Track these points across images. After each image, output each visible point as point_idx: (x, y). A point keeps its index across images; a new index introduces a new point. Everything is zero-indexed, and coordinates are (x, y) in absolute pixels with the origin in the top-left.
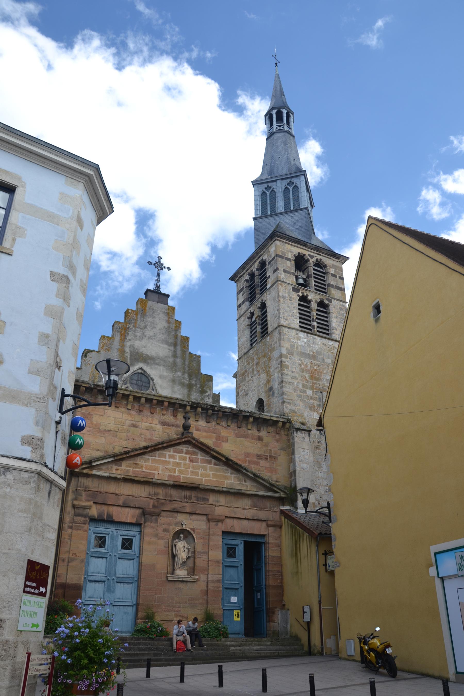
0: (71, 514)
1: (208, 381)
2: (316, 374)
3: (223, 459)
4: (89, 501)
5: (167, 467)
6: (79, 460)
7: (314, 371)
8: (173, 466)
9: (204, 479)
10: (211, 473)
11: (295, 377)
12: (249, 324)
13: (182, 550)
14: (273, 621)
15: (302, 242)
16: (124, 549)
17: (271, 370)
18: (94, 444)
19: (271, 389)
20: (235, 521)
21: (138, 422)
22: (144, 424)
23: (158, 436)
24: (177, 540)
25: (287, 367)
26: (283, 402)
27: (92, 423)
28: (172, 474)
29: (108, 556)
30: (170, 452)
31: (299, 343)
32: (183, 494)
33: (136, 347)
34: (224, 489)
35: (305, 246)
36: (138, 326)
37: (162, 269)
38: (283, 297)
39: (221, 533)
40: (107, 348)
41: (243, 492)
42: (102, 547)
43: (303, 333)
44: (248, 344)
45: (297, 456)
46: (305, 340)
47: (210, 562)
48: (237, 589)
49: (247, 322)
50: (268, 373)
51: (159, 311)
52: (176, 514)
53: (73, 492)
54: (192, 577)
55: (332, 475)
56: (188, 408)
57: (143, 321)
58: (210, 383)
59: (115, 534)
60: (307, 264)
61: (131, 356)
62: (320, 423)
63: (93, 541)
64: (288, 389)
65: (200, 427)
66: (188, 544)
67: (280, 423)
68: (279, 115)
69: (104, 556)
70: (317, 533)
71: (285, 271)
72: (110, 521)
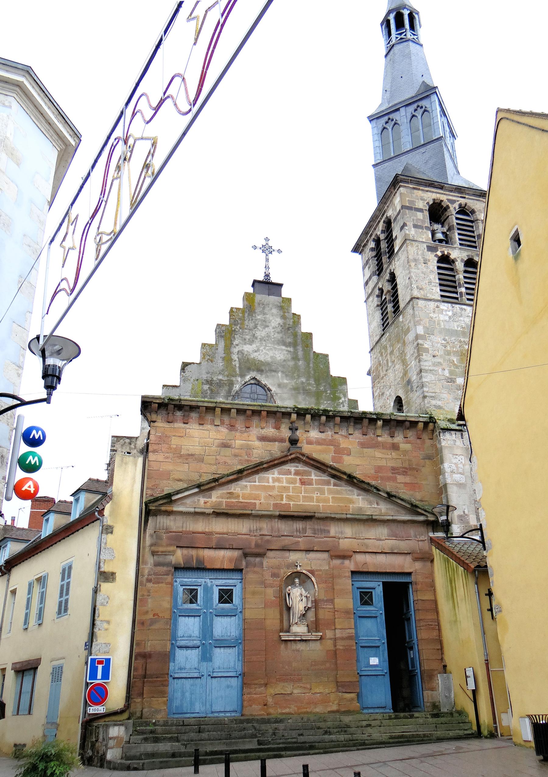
1: (341, 385)
3: (345, 477)
4: (171, 545)
5: (271, 493)
6: (32, 486)
8: (278, 492)
9: (321, 504)
10: (330, 496)
12: (379, 303)
15: (436, 184)
16: (221, 603)
18: (176, 474)
19: (409, 382)
22: (238, 443)
24: (290, 587)
25: (427, 351)
26: (425, 397)
27: (170, 448)
30: (273, 474)
32: (295, 527)
35: (442, 188)
37: (271, 253)
38: (415, 260)
39: (350, 573)
43: (446, 304)
45: (446, 465)
46: (450, 313)
47: (336, 613)
50: (404, 362)
52: (287, 554)
53: (151, 536)
55: (480, 484)
56: (294, 416)
57: (252, 320)
59: (209, 585)
60: (446, 213)
61: (240, 364)
64: (427, 378)
66: (306, 591)
67: (420, 424)
68: (399, 18)
70: (473, 567)
71: (415, 226)
72: (200, 568)
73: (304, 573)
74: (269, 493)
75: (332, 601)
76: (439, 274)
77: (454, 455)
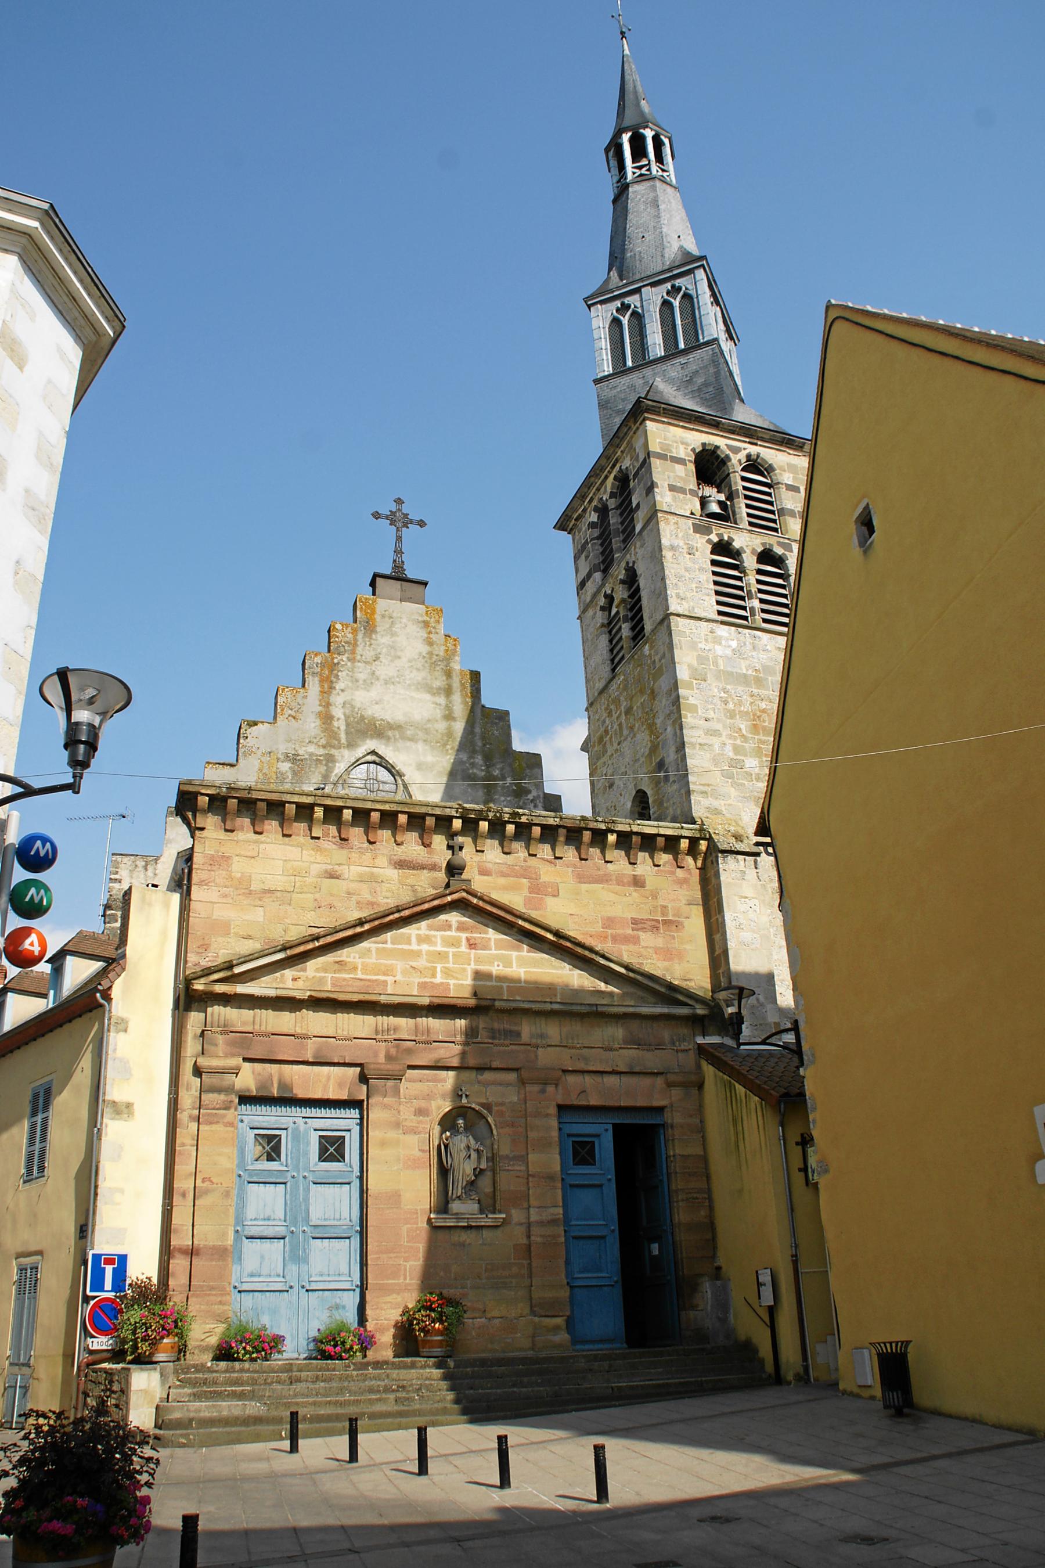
0: (194, 1090)
2: (764, 721)
4: (233, 1055)
5: (414, 964)
6: (36, 943)
7: (758, 714)
8: (428, 961)
11: (716, 731)
12: (606, 622)
13: (464, 1154)
14: (694, 1307)
17: (658, 721)
19: (661, 766)
20: (588, 1079)
21: (340, 865)
22: (356, 870)
23: (389, 894)
28: (427, 980)
29: (289, 1178)
30: (419, 929)
31: (719, 650)
33: (358, 705)
34: (556, 1007)
36: (358, 657)
38: (673, 548)
39: (556, 1109)
40: (292, 713)
41: (600, 1009)
42: (274, 1160)
44: (608, 668)
47: (531, 1179)
48: (603, 1237)
49: (600, 618)
50: (651, 727)
51: (404, 620)
54: (490, 1216)
58: (536, 770)
59: (302, 1126)
61: (348, 725)
62: (763, 829)
63: (253, 1149)
65: (490, 866)
66: (476, 1139)
69: (278, 1181)
71: (672, 488)
73: (474, 1109)
74: (411, 963)
75: (524, 1159)
76: (714, 573)
77: (742, 897)
